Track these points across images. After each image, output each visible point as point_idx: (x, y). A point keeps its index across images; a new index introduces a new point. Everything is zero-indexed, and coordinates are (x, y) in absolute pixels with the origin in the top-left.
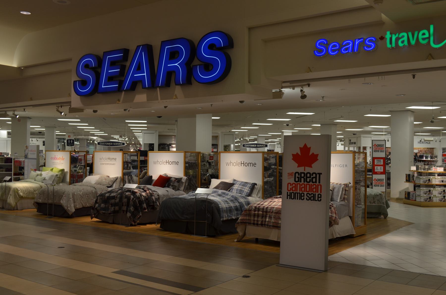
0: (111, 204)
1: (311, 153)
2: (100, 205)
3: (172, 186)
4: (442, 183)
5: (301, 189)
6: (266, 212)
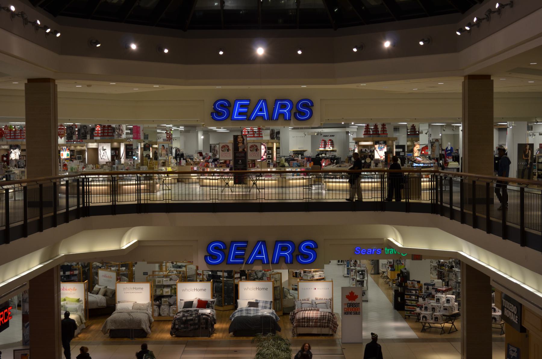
0: (190, 324)
2: (179, 326)
3: (211, 307)
4: (320, 278)
5: (350, 310)
6: (309, 320)
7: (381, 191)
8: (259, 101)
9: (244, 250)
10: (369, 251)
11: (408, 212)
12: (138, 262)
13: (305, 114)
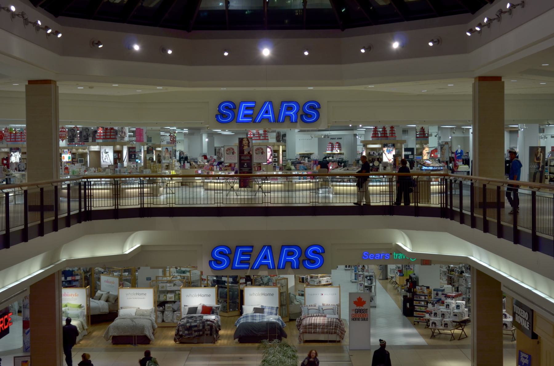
1: (362, 301)
2: (184, 332)
3: (216, 313)
5: (358, 316)
6: (316, 326)
7: (390, 195)
8: (265, 103)
9: (250, 255)
10: (377, 256)
11: (417, 216)
12: (141, 267)
13: (311, 116)
